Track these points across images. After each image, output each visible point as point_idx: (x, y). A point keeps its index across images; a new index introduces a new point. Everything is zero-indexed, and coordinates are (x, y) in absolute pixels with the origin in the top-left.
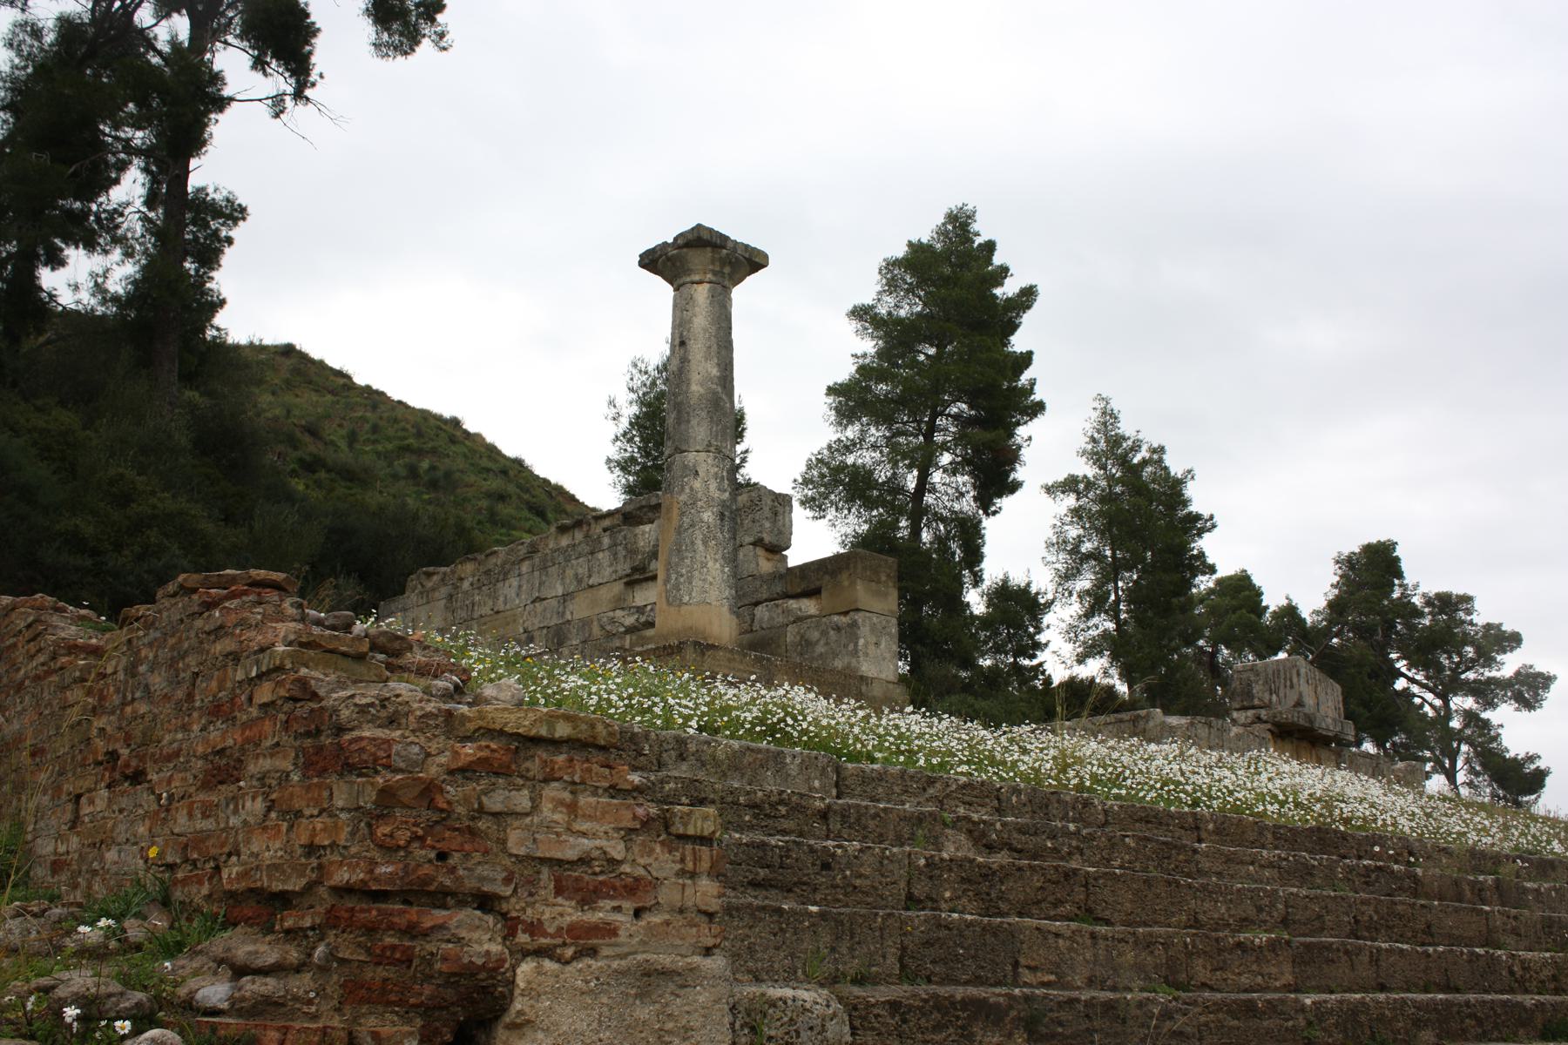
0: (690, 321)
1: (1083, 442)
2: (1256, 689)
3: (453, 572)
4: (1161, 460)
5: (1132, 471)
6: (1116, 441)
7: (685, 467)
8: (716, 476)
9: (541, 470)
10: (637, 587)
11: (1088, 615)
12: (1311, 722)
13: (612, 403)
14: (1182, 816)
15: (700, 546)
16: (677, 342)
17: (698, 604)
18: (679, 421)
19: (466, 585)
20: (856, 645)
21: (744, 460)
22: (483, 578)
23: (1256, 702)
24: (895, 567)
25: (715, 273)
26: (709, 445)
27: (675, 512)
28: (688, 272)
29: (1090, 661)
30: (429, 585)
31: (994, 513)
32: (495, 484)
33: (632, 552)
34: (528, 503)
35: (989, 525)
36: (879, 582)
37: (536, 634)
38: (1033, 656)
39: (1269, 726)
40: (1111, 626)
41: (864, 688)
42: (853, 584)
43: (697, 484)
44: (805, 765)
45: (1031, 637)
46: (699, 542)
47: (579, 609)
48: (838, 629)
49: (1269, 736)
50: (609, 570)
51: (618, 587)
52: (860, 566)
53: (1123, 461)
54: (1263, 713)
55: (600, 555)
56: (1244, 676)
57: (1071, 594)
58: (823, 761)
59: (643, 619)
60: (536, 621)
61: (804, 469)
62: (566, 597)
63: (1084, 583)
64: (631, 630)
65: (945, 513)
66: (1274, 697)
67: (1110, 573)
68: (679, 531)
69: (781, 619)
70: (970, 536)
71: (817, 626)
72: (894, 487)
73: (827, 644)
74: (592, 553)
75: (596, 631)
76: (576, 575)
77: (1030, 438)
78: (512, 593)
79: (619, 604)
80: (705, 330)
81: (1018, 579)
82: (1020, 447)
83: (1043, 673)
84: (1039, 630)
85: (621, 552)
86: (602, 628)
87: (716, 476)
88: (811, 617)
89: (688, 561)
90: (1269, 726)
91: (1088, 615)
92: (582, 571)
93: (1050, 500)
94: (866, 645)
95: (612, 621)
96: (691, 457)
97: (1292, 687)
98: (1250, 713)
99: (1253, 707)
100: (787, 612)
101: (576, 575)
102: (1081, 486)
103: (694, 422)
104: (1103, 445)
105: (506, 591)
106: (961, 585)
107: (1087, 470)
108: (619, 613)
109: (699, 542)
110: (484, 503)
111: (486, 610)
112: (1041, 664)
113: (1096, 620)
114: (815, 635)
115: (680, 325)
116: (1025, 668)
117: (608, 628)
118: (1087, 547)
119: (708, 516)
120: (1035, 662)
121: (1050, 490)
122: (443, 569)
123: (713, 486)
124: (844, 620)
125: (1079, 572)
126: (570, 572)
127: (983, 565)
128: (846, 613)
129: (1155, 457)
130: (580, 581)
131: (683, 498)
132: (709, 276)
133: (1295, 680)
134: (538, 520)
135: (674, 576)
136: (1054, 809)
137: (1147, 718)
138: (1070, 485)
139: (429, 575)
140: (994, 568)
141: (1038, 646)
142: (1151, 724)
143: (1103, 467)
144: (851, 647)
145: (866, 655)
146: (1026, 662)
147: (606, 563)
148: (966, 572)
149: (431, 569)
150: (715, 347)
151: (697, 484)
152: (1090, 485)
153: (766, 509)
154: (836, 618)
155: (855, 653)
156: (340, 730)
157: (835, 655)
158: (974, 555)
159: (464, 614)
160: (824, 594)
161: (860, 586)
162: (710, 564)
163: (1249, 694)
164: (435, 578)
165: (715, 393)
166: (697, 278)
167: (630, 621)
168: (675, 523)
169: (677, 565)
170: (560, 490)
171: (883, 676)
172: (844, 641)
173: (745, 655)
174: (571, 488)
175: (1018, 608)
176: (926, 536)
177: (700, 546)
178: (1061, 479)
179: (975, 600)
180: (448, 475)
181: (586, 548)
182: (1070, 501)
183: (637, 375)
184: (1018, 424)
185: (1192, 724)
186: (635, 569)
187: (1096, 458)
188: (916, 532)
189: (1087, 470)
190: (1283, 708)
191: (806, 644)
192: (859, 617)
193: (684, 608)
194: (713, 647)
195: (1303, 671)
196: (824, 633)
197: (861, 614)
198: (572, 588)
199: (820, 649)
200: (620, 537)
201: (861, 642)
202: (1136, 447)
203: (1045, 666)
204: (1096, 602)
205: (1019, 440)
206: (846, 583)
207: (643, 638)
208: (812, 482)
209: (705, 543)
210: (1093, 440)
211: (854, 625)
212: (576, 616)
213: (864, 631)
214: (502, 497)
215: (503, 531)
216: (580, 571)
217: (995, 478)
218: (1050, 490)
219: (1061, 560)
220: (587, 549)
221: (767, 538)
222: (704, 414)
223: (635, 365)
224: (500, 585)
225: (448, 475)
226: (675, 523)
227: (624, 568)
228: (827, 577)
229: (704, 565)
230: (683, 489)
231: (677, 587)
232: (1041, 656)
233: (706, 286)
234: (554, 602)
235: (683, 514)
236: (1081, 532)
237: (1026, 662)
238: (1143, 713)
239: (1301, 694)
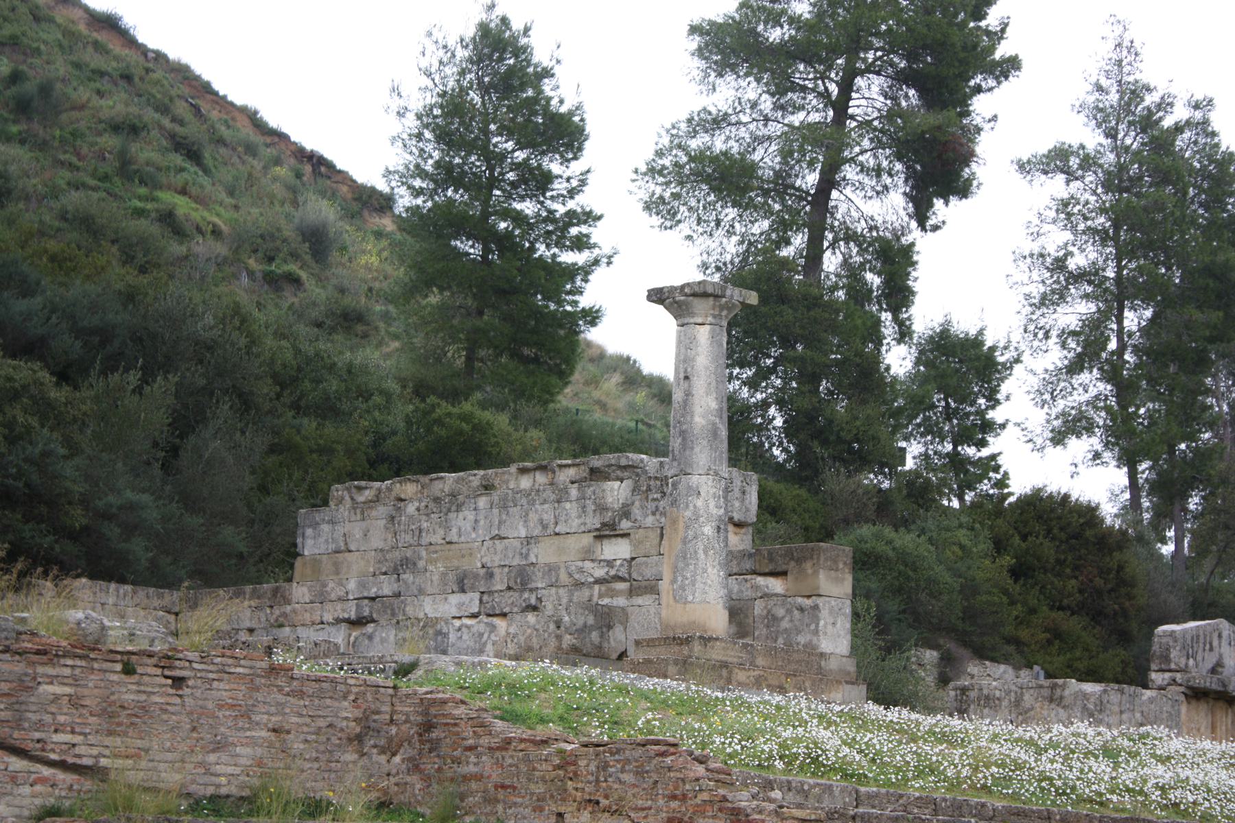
0: (693, 360)
1: (1082, 92)
2: (1174, 654)
3: (389, 489)
4: (1206, 122)
5: (1160, 142)
6: (1133, 93)
7: (690, 487)
8: (714, 496)
9: (148, 36)
10: (605, 542)
11: (1075, 367)
12: (1224, 686)
13: (396, 91)
14: (1039, 811)
15: (701, 555)
16: (682, 376)
17: (700, 602)
18: (684, 446)
19: (411, 509)
20: (817, 625)
21: (583, 183)
22: (432, 505)
23: (1173, 666)
24: (851, 554)
25: (714, 316)
26: (710, 469)
27: (681, 525)
28: (692, 315)
29: (1073, 442)
30: (361, 499)
31: (936, 228)
32: (116, 104)
33: (601, 508)
34: (172, 136)
35: (925, 245)
36: (837, 570)
37: (497, 571)
38: (982, 444)
39: (1182, 689)
40: (1105, 388)
41: (823, 663)
42: (816, 573)
43: (700, 503)
44: (842, 791)
45: (981, 413)
46: (701, 552)
47: (543, 553)
48: (801, 609)
49: (1182, 698)
50: (576, 522)
51: (587, 539)
52: (822, 558)
53: (1147, 123)
54: (1178, 676)
55: (568, 505)
56: (1164, 640)
57: (1047, 336)
58: (850, 788)
59: (612, 572)
60: (496, 558)
61: (650, 155)
62: (529, 540)
63: (1075, 311)
64: (598, 581)
65: (861, 227)
66: (1191, 662)
67: (1116, 298)
68: (685, 541)
69: (749, 593)
70: (895, 259)
71: (783, 605)
72: (782, 184)
73: (791, 621)
74: (559, 502)
75: (563, 577)
76: (541, 521)
77: (994, 118)
78: (468, 526)
79: (588, 555)
80: (707, 368)
81: (965, 325)
82: (979, 130)
83: (997, 469)
84: (994, 402)
85: (591, 507)
86: (570, 575)
87: (714, 496)
88: (776, 595)
89: (692, 567)
90: (1182, 689)
91: (1075, 367)
92: (549, 517)
93: (1025, 183)
94: (825, 626)
95: (581, 570)
96: (694, 480)
97: (1211, 649)
98: (1167, 675)
99: (1170, 671)
100: (756, 587)
101: (541, 521)
102: (1074, 162)
103: (697, 449)
104: (1114, 97)
105: (460, 523)
106: (878, 341)
107: (1092, 139)
108: (588, 564)
109: (701, 552)
110: (110, 141)
111: (437, 538)
112: (993, 457)
113: (1085, 377)
114: (780, 612)
115: (685, 361)
116: (968, 460)
117: (577, 576)
118: (1077, 261)
119: (708, 530)
120: (985, 452)
121: (1023, 167)
122: (377, 484)
123: (712, 504)
124: (808, 602)
125: (1062, 297)
126: (533, 517)
127: (913, 310)
128: (809, 597)
129: (1198, 115)
130: (545, 527)
131: (688, 514)
132: (710, 319)
133: (1215, 643)
134: (192, 168)
135: (680, 579)
136: (965, 809)
137: (1063, 687)
138: (1058, 160)
139: (359, 489)
140: (924, 316)
141: (989, 427)
142: (1067, 692)
143: (1111, 134)
144: (813, 627)
145: (825, 633)
146: (971, 451)
147: (574, 514)
148: (886, 316)
149: (363, 483)
150: (714, 384)
151: (700, 503)
152: (1088, 162)
153: (736, 490)
154: (800, 600)
155: (816, 632)
156: (747, 815)
157: (799, 632)
158: (899, 295)
159: (408, 538)
160: (790, 577)
161: (822, 576)
162: (710, 570)
163: (1166, 659)
164: (367, 492)
165: (714, 424)
166: (700, 320)
167: (600, 573)
168: (681, 534)
169: (683, 569)
170: (182, 73)
171: (838, 651)
172: (806, 620)
173: (735, 644)
174: (204, 69)
175: (964, 367)
176: (831, 262)
177: (701, 555)
178: (1043, 150)
179: (898, 360)
180: (45, 90)
181: (549, 494)
182: (1057, 186)
183: (430, 47)
184: (978, 90)
185: (1105, 691)
186: (604, 525)
187: (1102, 118)
188: (814, 255)
189: (1092, 139)
190: (1200, 675)
191: (772, 619)
192: (820, 601)
193: (688, 606)
194: (710, 639)
195: (1225, 634)
196: (789, 611)
197: (822, 599)
198: (536, 533)
199: (785, 624)
200: (589, 491)
201: (822, 623)
202: (1165, 105)
203: (1000, 460)
204: (1088, 349)
205: (978, 121)
206: (810, 571)
207: (613, 590)
208: (660, 173)
209: (706, 552)
210: (1099, 88)
211: (816, 607)
212: (542, 560)
213: (824, 613)
214: (133, 129)
215: (143, 191)
216: (545, 517)
217: (938, 167)
218: (1023, 167)
219: (1036, 282)
220: (553, 497)
221: (736, 517)
222: (705, 443)
223: (430, 34)
224: (452, 515)
225: (45, 90)
226: (681, 534)
227: (594, 522)
228: (793, 563)
229: (705, 571)
230: (687, 506)
231: (683, 588)
232: (995, 444)
233: (708, 327)
234: (517, 543)
235: (687, 527)
236: (1068, 236)
237: (971, 451)
238: (1060, 681)
239: (1221, 655)
